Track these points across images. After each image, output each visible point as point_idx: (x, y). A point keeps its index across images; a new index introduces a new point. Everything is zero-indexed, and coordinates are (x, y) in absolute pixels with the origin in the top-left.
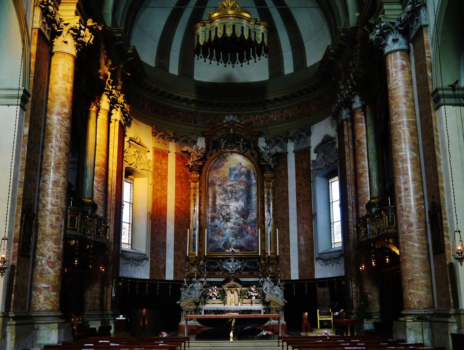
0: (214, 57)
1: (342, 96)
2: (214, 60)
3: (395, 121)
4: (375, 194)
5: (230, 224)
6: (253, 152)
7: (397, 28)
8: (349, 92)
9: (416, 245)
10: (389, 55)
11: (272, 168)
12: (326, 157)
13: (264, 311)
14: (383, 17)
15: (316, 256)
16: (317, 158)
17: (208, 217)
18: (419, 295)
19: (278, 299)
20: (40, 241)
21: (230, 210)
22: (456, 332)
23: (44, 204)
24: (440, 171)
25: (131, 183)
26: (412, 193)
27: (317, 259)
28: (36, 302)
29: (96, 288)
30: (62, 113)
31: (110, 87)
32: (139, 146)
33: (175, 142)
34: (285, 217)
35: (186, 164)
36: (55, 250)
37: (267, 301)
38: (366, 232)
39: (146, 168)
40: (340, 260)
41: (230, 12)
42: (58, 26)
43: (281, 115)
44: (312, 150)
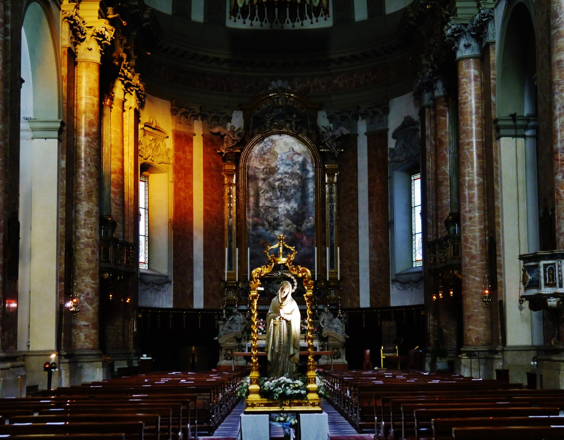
0: (257, 16)
2: (257, 20)
3: (462, 141)
6: (310, 131)
10: (461, 62)
11: (336, 156)
12: (407, 147)
13: (321, 348)
14: (453, 18)
16: (396, 146)
17: (249, 223)
18: (477, 332)
19: (337, 333)
20: (77, 276)
21: (279, 213)
22: (501, 368)
23: (78, 237)
24: (497, 206)
25: (145, 182)
27: (394, 281)
28: (76, 340)
30: (91, 133)
31: (126, 71)
32: (156, 132)
33: (202, 120)
34: (353, 223)
35: (218, 151)
36: (92, 285)
37: (324, 336)
38: (435, 260)
39: (165, 160)
40: (420, 284)
42: (81, 32)
44: (390, 134)
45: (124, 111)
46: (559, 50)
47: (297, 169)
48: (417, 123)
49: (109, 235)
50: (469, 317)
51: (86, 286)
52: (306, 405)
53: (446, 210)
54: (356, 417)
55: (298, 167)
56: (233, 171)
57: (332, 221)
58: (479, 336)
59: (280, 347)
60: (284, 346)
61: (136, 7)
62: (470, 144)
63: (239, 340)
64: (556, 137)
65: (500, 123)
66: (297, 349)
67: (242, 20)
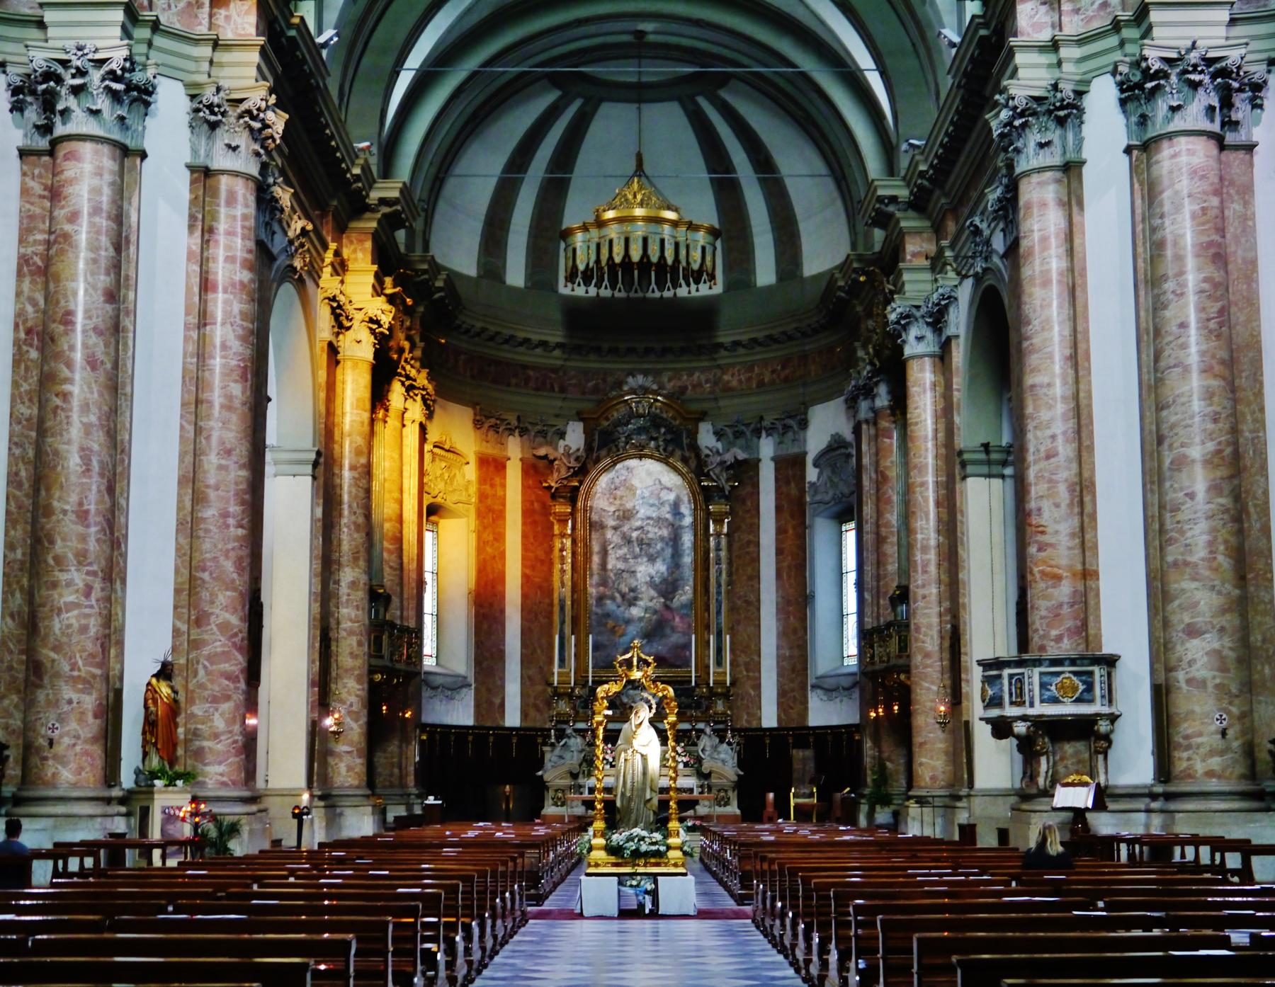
0: (606, 282)
5: (636, 612)
6: (687, 454)
15: (811, 681)
18: (933, 768)
27: (814, 687)
29: (393, 747)
31: (408, 367)
38: (872, 657)
39: (464, 499)
41: (639, 212)
42: (347, 317)
43: (748, 375)
44: (810, 460)
45: (404, 426)
46: (1032, 371)
47: (666, 512)
49: (381, 617)
50: (921, 745)
51: (349, 693)
52: (666, 865)
53: (893, 580)
54: (735, 884)
55: (668, 509)
56: (565, 514)
57: (719, 593)
61: (425, 272)
62: (923, 484)
63: (574, 776)
64: (1029, 492)
65: (966, 456)
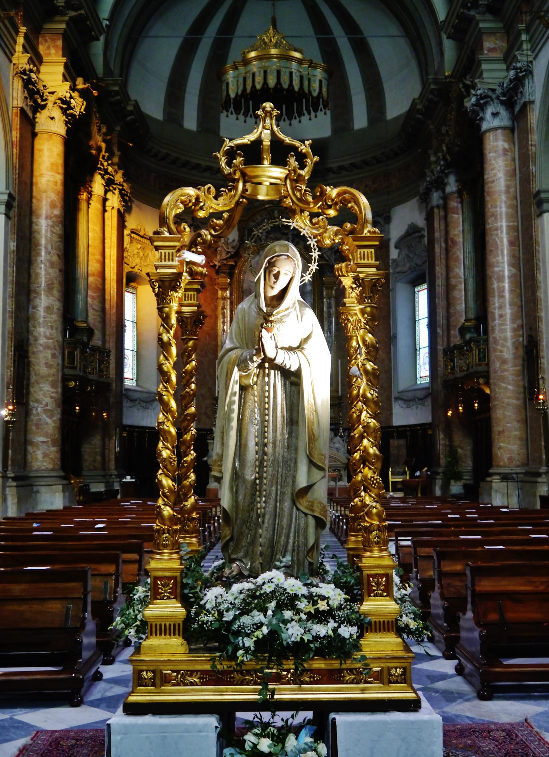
1: (432, 172)
3: (491, 225)
4: (472, 316)
7: (498, 97)
8: (441, 169)
9: (510, 387)
10: (487, 134)
12: (411, 256)
15: (394, 394)
16: (399, 256)
20: (33, 383)
26: (508, 322)
27: (397, 399)
29: (97, 440)
31: (105, 164)
35: (211, 264)
38: (453, 368)
41: (274, 51)
42: (42, 97)
48: (423, 229)
50: (500, 433)
53: (461, 316)
58: (512, 455)
59: (261, 462)
60: (275, 460)
66: (321, 469)
67: (234, 116)
